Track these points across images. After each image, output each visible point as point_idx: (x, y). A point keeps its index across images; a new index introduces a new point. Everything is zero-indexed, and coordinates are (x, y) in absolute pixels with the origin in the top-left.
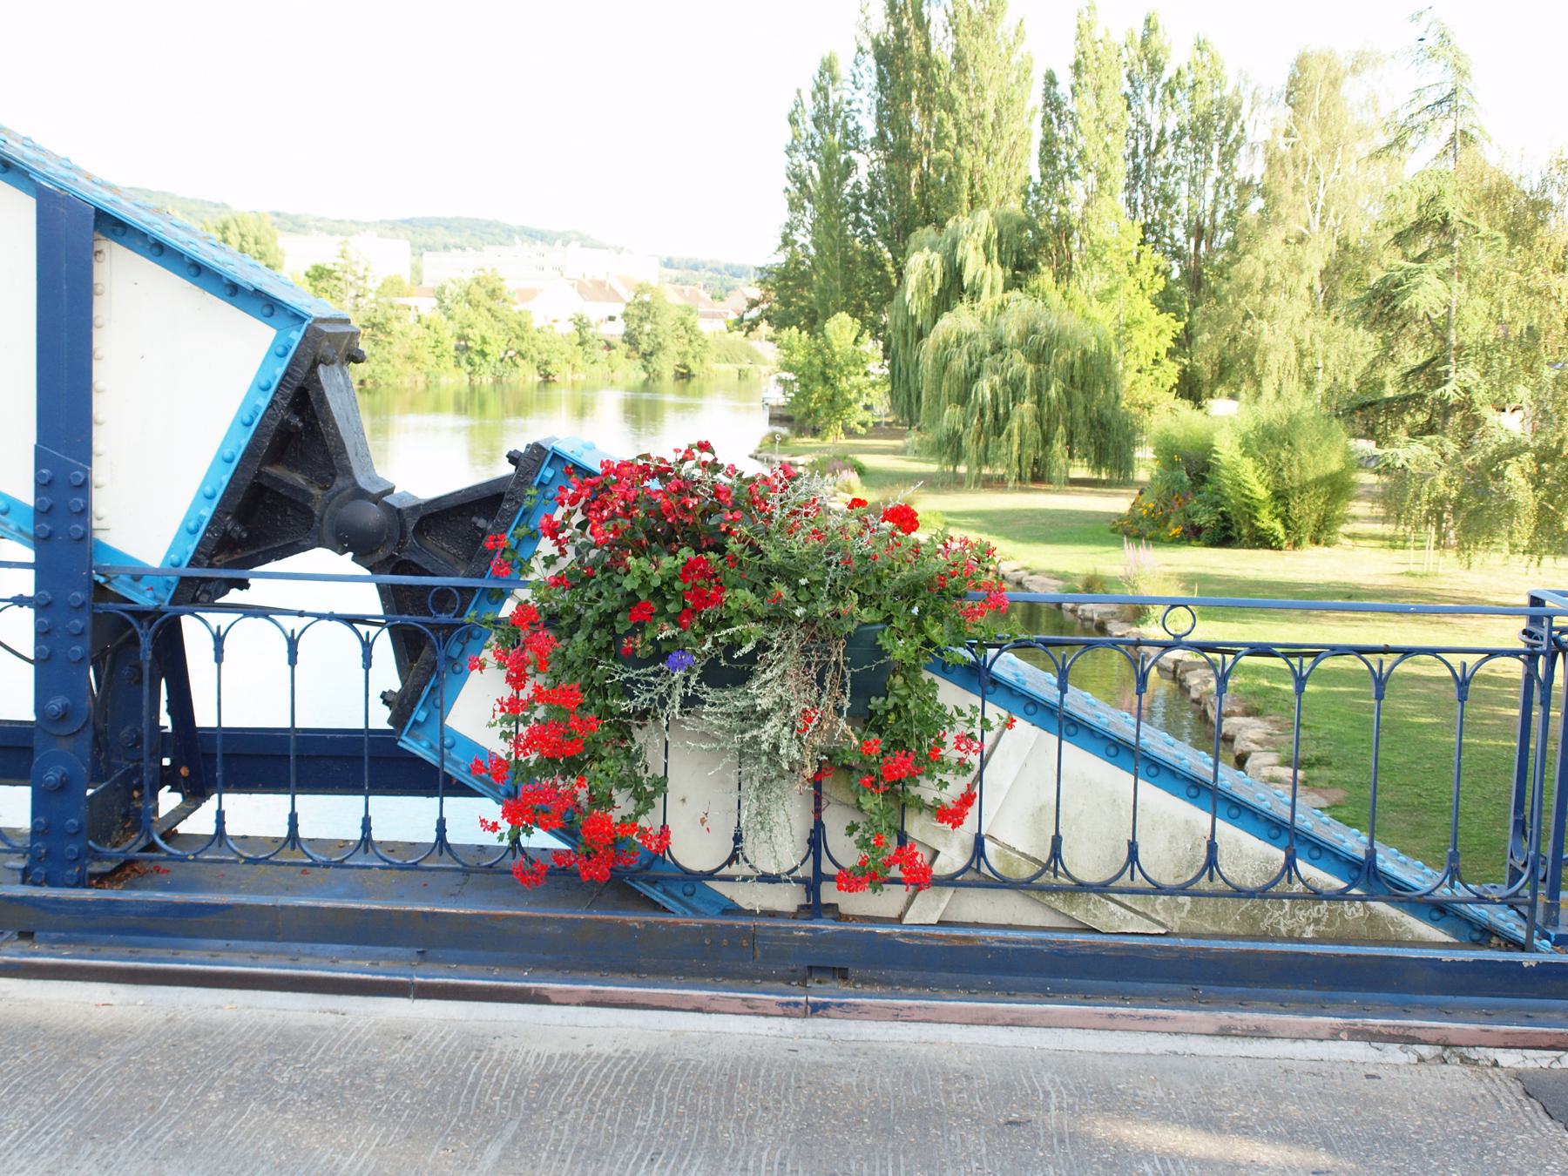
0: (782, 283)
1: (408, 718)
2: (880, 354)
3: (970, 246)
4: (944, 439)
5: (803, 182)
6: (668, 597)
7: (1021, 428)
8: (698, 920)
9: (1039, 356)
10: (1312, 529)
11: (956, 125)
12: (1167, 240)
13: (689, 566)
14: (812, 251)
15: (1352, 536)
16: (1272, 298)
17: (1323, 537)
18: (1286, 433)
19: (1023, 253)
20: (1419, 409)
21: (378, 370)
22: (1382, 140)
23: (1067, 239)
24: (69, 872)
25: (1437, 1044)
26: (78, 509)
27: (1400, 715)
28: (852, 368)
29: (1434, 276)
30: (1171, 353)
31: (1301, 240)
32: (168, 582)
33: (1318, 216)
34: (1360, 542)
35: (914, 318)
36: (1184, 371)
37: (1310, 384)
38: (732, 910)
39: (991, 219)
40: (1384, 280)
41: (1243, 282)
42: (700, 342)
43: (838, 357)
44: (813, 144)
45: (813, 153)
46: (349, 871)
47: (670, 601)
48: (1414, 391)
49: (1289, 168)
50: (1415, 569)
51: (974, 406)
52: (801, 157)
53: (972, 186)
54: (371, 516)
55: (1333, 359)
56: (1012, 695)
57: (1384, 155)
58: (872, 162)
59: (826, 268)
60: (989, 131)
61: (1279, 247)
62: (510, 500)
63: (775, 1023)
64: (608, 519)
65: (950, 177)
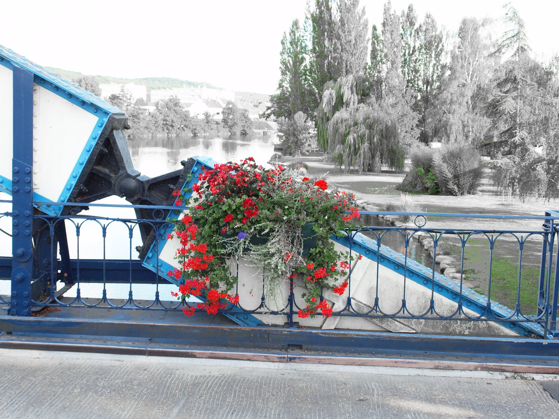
1: (146, 256)
3: (346, 88)
5: (286, 65)
7: (364, 153)
9: (370, 127)
10: (468, 188)
11: (341, 44)
14: (290, 89)
15: (482, 191)
16: (453, 106)
17: (472, 191)
18: (459, 154)
19: (364, 90)
20: (506, 146)
21: (135, 132)
22: (493, 50)
23: (380, 85)
24: (25, 311)
25: (512, 372)
26: (28, 182)
28: (304, 131)
29: (511, 98)
32: (60, 207)
34: (485, 193)
35: (326, 114)
36: (422, 132)
38: (261, 324)
40: (493, 100)
41: (443, 101)
42: (250, 122)
43: (299, 127)
44: (290, 51)
45: (290, 54)
49: (460, 60)
50: (504, 203)
52: (286, 56)
53: (347, 66)
54: (132, 184)
55: (475, 128)
58: (311, 58)
61: (456, 89)
62: (182, 178)
63: (276, 364)
64: (217, 185)
65: (338, 64)
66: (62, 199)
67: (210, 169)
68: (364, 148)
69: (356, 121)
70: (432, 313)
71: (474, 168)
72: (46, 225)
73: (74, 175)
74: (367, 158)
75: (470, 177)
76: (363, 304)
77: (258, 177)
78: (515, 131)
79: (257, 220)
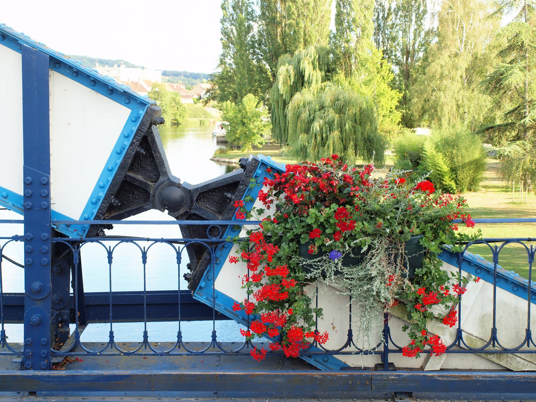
0: (221, 81)
1: (197, 286)
2: (267, 112)
3: (306, 62)
4: (299, 149)
5: (229, 36)
6: (326, 226)
7: (333, 143)
8: (346, 373)
9: (340, 111)
10: (468, 184)
11: (297, 8)
12: (393, 57)
13: (337, 214)
14: (234, 66)
15: (485, 187)
16: (445, 82)
17: (473, 187)
18: (455, 141)
19: (330, 65)
20: (513, 129)
22: (491, 11)
23: (349, 58)
24: (43, 363)
26: (45, 195)
27: (518, 266)
28: (255, 119)
29: (518, 70)
30: (397, 108)
31: (456, 55)
32: (85, 227)
33: (463, 44)
34: (489, 190)
35: (282, 95)
36: (403, 115)
37: (462, 119)
38: (345, 368)
39: (315, 50)
40: (496, 72)
41: (431, 75)
42: (182, 108)
43: (248, 114)
44: (233, 18)
45: (233, 22)
46: (172, 357)
47: (328, 228)
48: (510, 121)
49: (450, 24)
50: (515, 201)
51: (312, 134)
52: (227, 24)
53: (305, 35)
54: (176, 194)
55: (472, 108)
56: (470, 265)
57: (494, 16)
58: (260, 26)
59: (240, 73)
60: (312, 10)
61: (447, 59)
62: (242, 184)
64: (298, 192)
65: (295, 32)
66: (86, 216)
67: (279, 172)
68: (334, 137)
69: (322, 104)
70: (528, 345)
71: (474, 159)
72: (68, 251)
73: (101, 184)
74: (337, 149)
75: (470, 170)
76: (474, 336)
77: (348, 180)
78: (524, 111)
79: (351, 235)
